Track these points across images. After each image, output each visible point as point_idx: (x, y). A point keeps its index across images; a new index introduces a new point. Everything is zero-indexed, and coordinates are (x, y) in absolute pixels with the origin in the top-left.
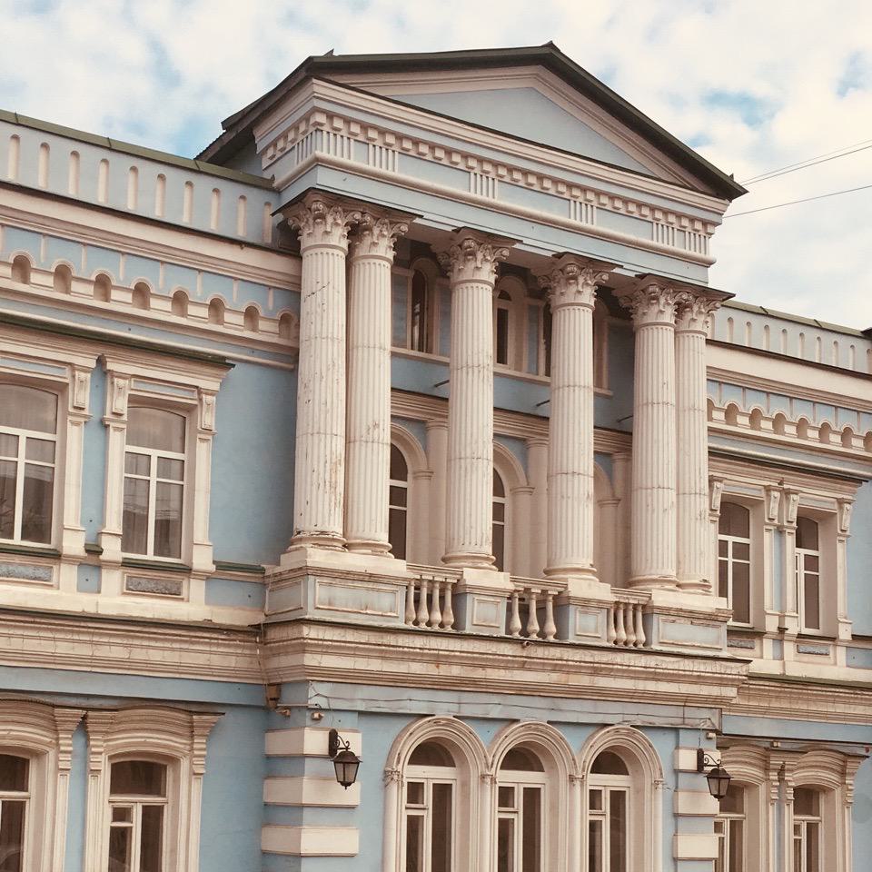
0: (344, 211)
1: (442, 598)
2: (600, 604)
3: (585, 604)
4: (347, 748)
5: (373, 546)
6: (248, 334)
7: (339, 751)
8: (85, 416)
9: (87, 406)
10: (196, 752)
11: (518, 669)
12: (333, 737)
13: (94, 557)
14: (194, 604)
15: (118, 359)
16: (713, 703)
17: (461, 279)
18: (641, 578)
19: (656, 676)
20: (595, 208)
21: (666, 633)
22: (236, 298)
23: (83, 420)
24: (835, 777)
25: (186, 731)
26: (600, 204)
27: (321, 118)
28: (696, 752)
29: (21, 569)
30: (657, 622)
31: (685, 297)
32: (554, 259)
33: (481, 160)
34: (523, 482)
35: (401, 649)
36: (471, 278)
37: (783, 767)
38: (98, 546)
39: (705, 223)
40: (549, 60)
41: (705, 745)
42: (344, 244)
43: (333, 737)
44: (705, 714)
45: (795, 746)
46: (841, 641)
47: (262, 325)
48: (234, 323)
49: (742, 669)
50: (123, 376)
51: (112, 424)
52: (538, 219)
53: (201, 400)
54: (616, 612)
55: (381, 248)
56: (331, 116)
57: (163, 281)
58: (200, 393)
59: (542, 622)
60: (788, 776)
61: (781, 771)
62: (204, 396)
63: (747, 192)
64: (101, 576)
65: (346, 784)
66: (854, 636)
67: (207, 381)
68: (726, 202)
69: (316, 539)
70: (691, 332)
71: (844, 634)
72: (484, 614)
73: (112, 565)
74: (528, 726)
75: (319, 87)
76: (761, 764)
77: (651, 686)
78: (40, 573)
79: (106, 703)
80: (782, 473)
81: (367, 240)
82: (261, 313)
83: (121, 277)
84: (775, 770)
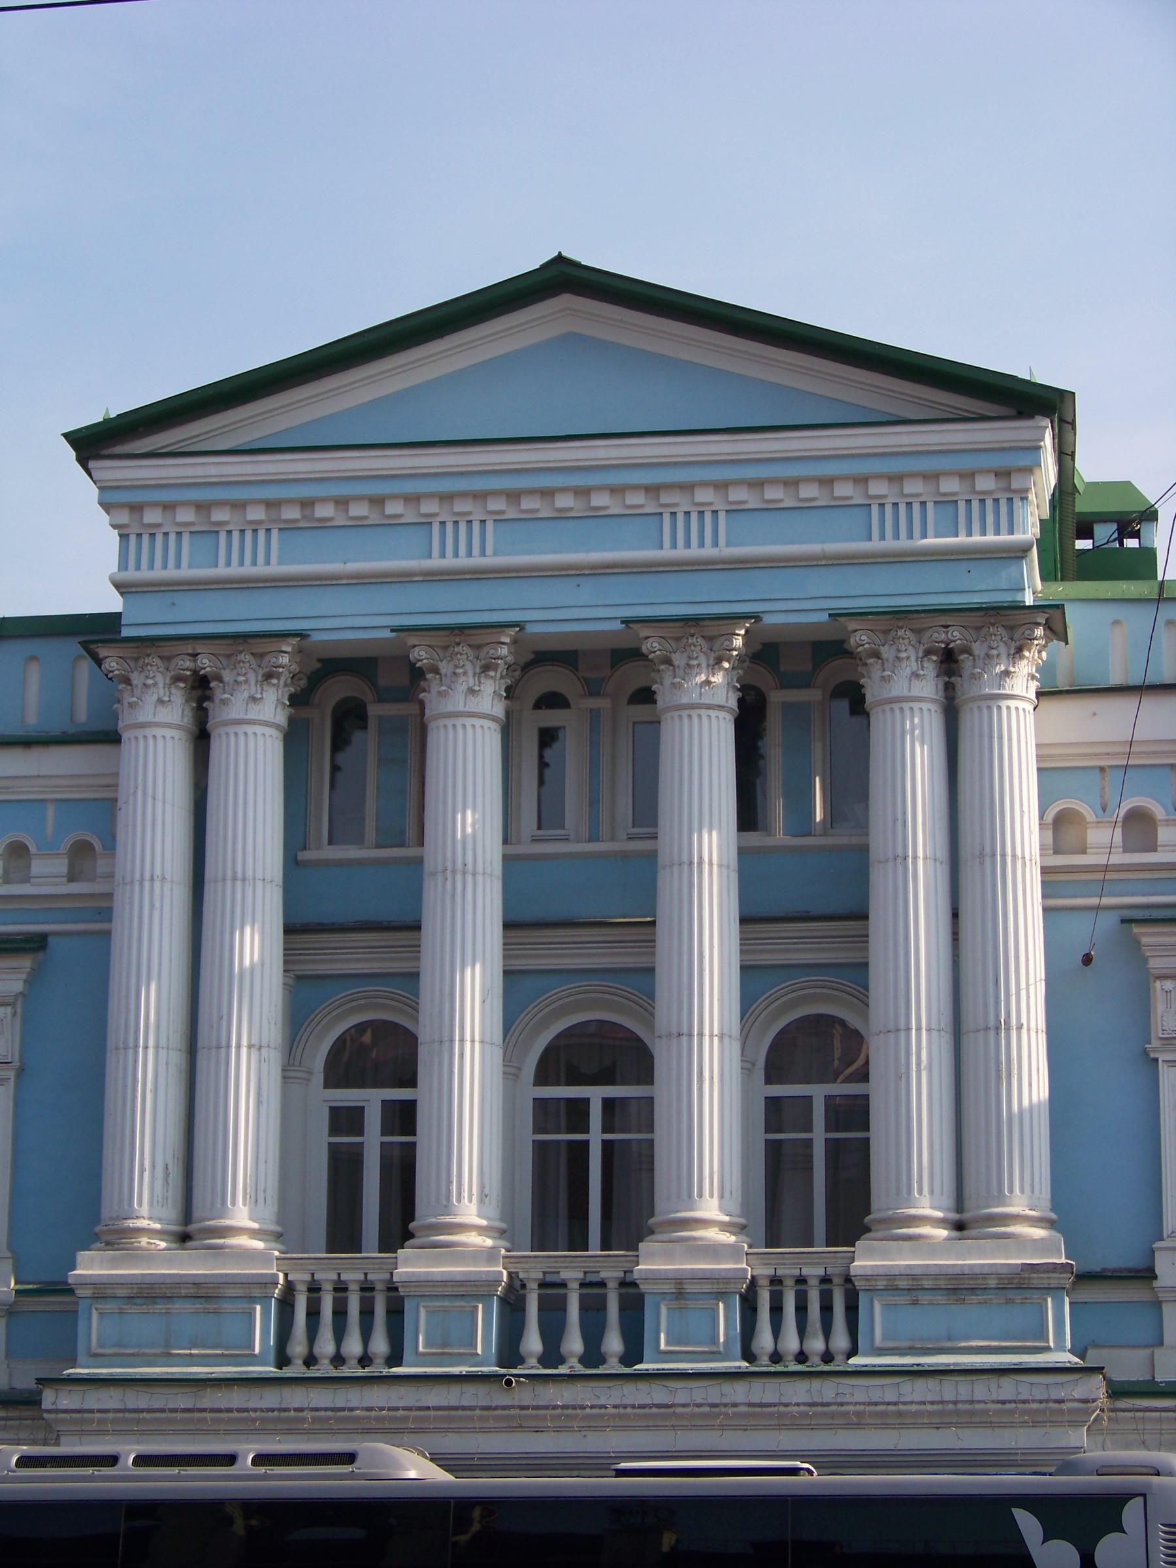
17: (885, 694)
35: (346, 1413)
36: (242, 716)
59: (340, 1333)
63: (62, 435)
82: (33, 849)
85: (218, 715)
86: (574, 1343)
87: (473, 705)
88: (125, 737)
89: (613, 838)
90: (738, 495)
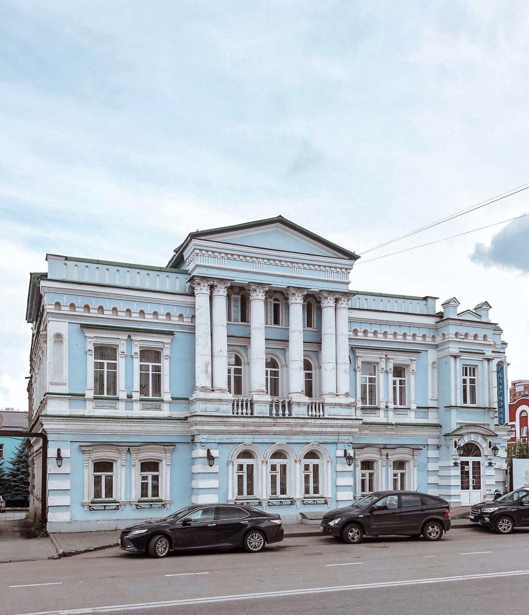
0: (333, 295)
1: (319, 407)
2: (304, 404)
3: (299, 404)
4: (349, 455)
5: (222, 390)
6: (181, 323)
7: (347, 456)
8: (125, 355)
9: (415, 370)
10: (167, 458)
11: (195, 425)
12: (208, 451)
13: (130, 399)
14: (165, 411)
15: (134, 335)
16: (349, 434)
18: (324, 393)
19: (326, 426)
20: (302, 269)
21: (329, 411)
22: (175, 311)
23: (124, 356)
24: (411, 457)
25: (164, 452)
26: (228, 258)
27: (197, 251)
28: (344, 451)
29: (106, 404)
30: (326, 408)
31: (337, 296)
32: (320, 292)
33: (257, 258)
34: (284, 363)
37: (387, 454)
38: (132, 395)
39: (346, 269)
40: (280, 220)
41: (347, 448)
42: (208, 292)
43: (208, 451)
44: (347, 438)
45: (394, 447)
46: (412, 409)
47: (185, 320)
48: (175, 320)
49: (361, 422)
50: (136, 341)
51: (134, 356)
52: (336, 282)
53: (164, 346)
54: (310, 406)
55: (221, 292)
56: (201, 250)
57: (149, 309)
58: (164, 344)
59: (284, 411)
60: (390, 457)
61: (387, 455)
62: (165, 345)
63: (360, 257)
64: (133, 405)
65: (350, 465)
66: (418, 408)
67: (166, 340)
68: (354, 261)
69: (200, 389)
70: (341, 308)
71: (413, 407)
72: (261, 409)
73: (90, 400)
74: (279, 445)
75: (194, 241)
76: (411, 454)
77: (324, 429)
78: (113, 405)
79: (137, 444)
80: (386, 352)
81: (216, 290)
82: (184, 316)
83: (149, 310)
84: (384, 455)
85: (215, 293)
86: (281, 412)
87: (342, 306)
88: (196, 296)
89: (282, 325)
90: (305, 266)
